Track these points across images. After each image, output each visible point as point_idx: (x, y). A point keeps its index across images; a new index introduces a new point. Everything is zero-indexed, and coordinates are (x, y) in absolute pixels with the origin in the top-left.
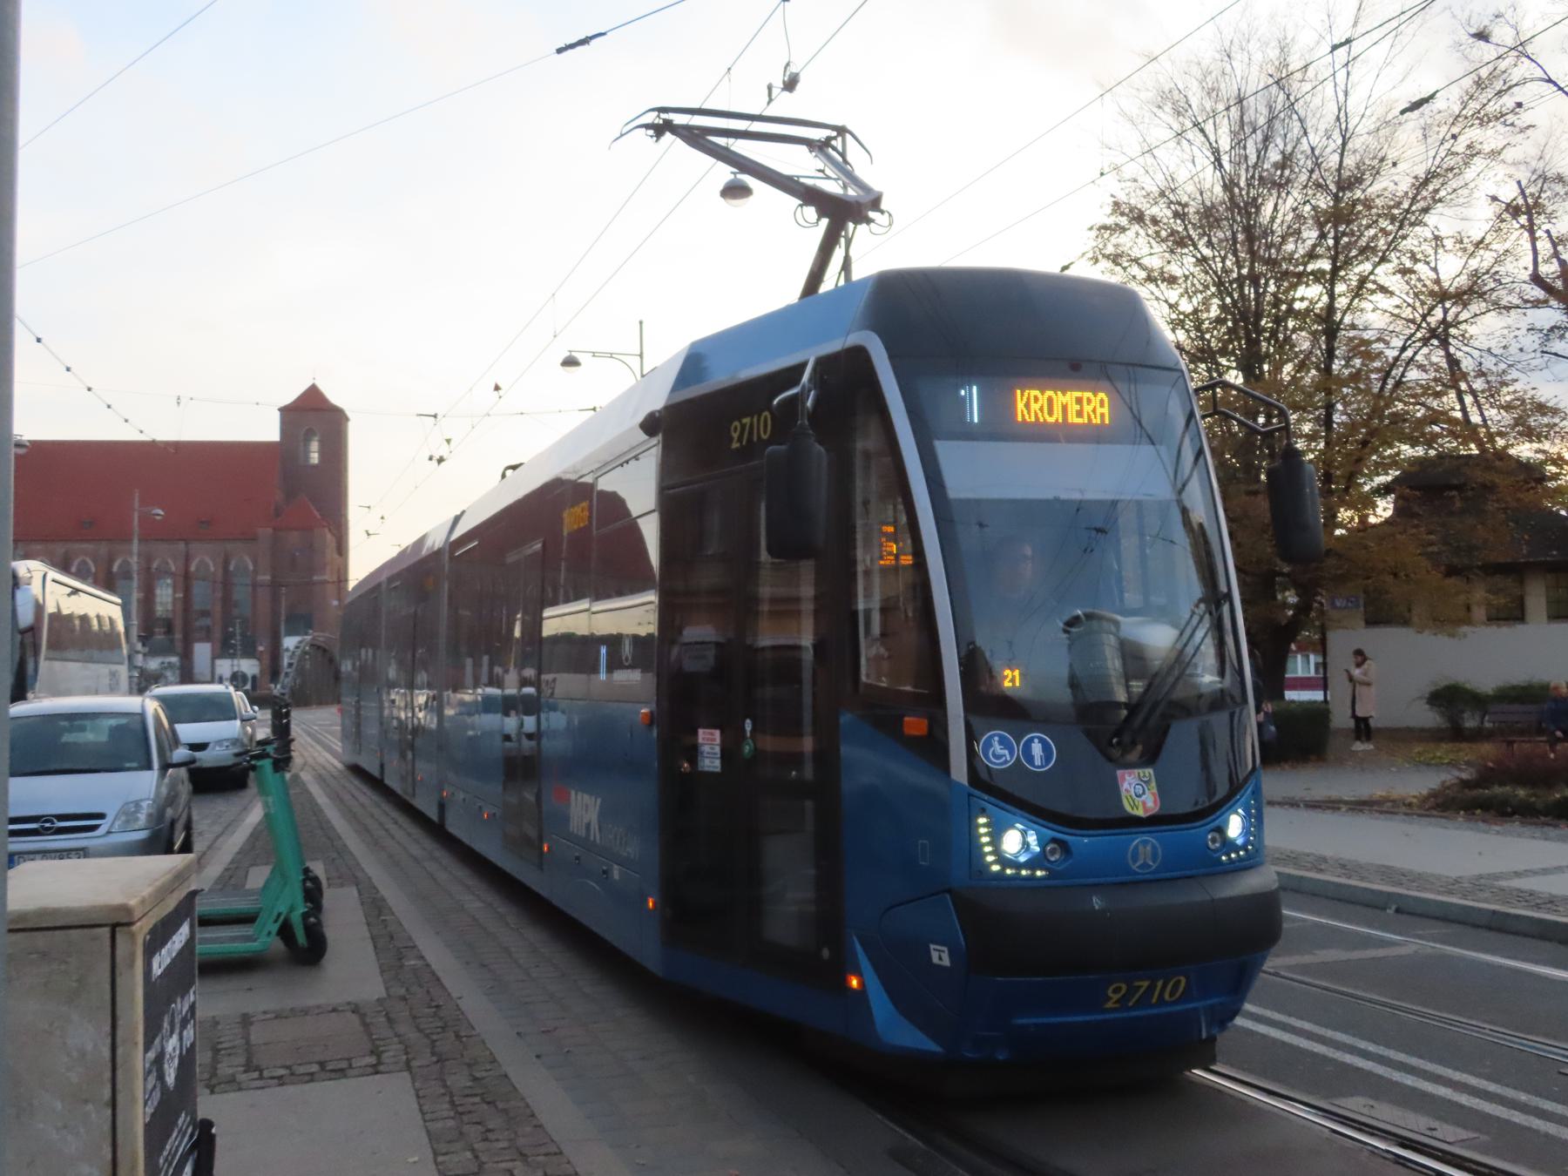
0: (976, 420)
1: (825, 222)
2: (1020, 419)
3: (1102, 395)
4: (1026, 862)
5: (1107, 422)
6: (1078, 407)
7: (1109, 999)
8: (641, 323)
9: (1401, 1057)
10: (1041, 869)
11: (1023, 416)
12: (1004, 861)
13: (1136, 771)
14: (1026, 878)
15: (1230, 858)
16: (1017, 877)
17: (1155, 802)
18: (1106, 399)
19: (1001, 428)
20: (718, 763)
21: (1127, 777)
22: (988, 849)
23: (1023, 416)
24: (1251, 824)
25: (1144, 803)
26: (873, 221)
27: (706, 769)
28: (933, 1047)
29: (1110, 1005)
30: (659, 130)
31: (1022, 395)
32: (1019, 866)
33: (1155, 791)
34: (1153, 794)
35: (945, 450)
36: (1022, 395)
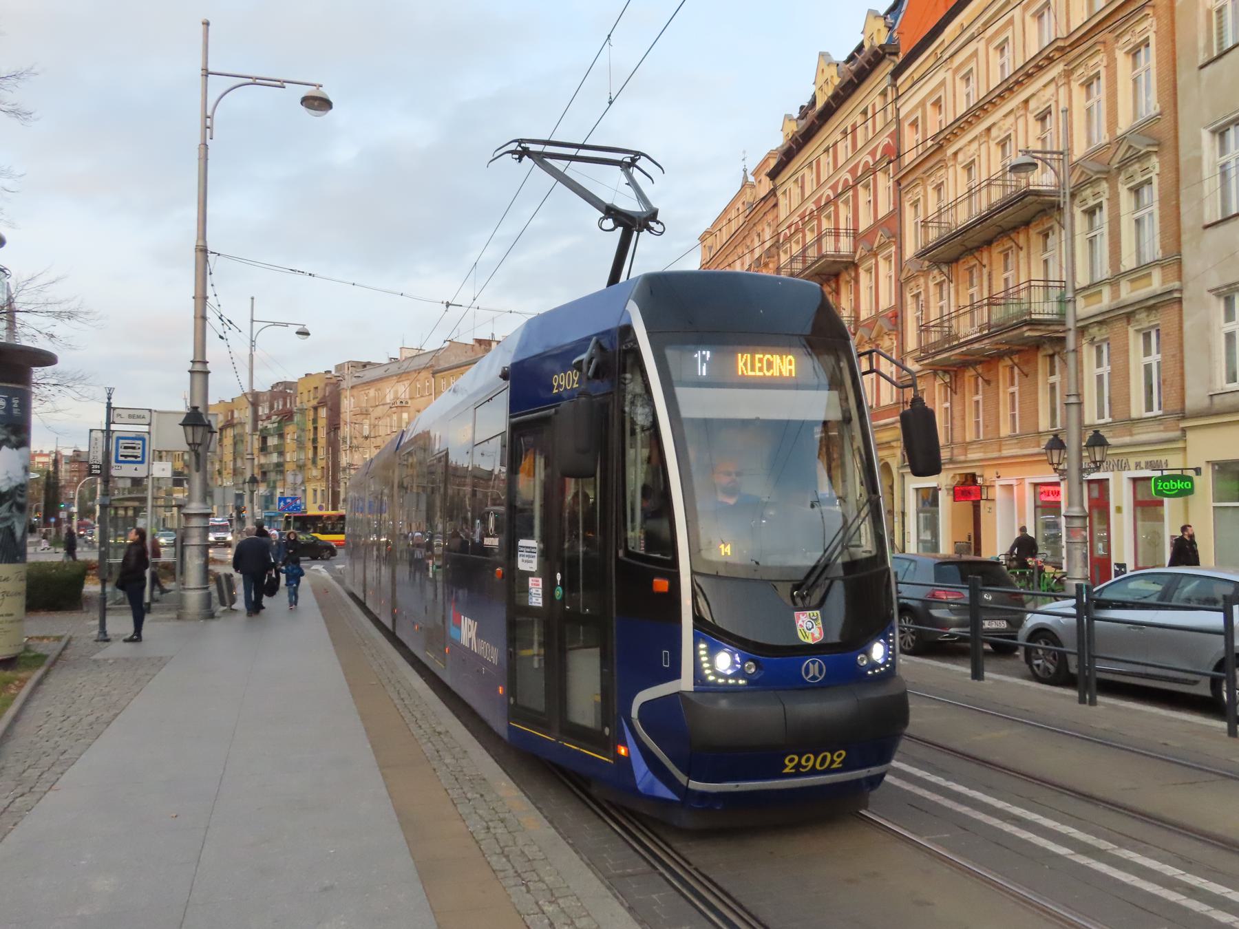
0: (704, 374)
1: (620, 230)
2: (740, 373)
3: (790, 357)
4: (731, 674)
5: (794, 375)
6: (760, 365)
7: (786, 766)
8: (253, 298)
9: (1000, 804)
10: (742, 679)
11: (742, 371)
12: (718, 674)
13: (808, 612)
14: (732, 685)
15: (874, 672)
16: (726, 684)
17: (820, 634)
18: (793, 360)
19: (721, 381)
20: (540, 600)
21: (801, 616)
22: (706, 665)
23: (742, 371)
24: (889, 650)
25: (813, 634)
26: (653, 229)
27: (533, 604)
28: (675, 797)
29: (787, 770)
30: (522, 153)
31: (742, 357)
32: (726, 677)
33: (821, 626)
34: (819, 628)
35: (681, 392)
36: (742, 357)
